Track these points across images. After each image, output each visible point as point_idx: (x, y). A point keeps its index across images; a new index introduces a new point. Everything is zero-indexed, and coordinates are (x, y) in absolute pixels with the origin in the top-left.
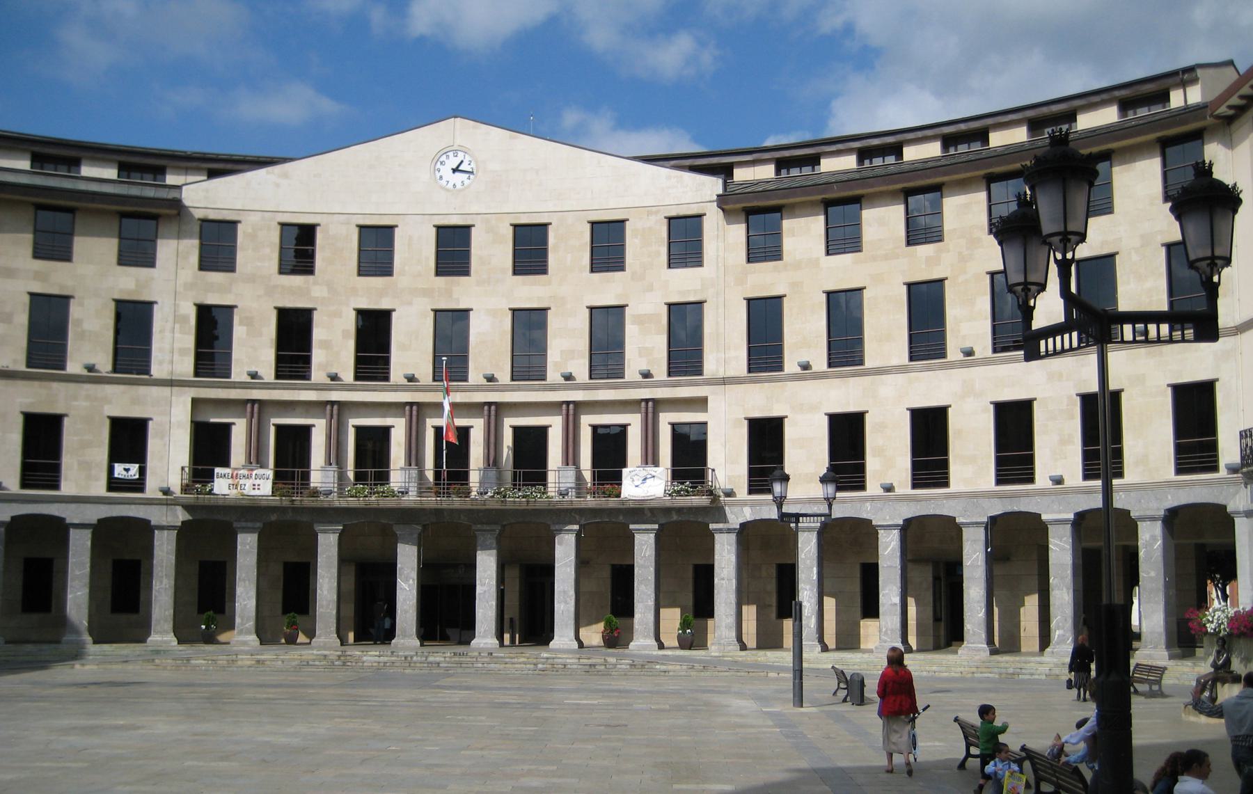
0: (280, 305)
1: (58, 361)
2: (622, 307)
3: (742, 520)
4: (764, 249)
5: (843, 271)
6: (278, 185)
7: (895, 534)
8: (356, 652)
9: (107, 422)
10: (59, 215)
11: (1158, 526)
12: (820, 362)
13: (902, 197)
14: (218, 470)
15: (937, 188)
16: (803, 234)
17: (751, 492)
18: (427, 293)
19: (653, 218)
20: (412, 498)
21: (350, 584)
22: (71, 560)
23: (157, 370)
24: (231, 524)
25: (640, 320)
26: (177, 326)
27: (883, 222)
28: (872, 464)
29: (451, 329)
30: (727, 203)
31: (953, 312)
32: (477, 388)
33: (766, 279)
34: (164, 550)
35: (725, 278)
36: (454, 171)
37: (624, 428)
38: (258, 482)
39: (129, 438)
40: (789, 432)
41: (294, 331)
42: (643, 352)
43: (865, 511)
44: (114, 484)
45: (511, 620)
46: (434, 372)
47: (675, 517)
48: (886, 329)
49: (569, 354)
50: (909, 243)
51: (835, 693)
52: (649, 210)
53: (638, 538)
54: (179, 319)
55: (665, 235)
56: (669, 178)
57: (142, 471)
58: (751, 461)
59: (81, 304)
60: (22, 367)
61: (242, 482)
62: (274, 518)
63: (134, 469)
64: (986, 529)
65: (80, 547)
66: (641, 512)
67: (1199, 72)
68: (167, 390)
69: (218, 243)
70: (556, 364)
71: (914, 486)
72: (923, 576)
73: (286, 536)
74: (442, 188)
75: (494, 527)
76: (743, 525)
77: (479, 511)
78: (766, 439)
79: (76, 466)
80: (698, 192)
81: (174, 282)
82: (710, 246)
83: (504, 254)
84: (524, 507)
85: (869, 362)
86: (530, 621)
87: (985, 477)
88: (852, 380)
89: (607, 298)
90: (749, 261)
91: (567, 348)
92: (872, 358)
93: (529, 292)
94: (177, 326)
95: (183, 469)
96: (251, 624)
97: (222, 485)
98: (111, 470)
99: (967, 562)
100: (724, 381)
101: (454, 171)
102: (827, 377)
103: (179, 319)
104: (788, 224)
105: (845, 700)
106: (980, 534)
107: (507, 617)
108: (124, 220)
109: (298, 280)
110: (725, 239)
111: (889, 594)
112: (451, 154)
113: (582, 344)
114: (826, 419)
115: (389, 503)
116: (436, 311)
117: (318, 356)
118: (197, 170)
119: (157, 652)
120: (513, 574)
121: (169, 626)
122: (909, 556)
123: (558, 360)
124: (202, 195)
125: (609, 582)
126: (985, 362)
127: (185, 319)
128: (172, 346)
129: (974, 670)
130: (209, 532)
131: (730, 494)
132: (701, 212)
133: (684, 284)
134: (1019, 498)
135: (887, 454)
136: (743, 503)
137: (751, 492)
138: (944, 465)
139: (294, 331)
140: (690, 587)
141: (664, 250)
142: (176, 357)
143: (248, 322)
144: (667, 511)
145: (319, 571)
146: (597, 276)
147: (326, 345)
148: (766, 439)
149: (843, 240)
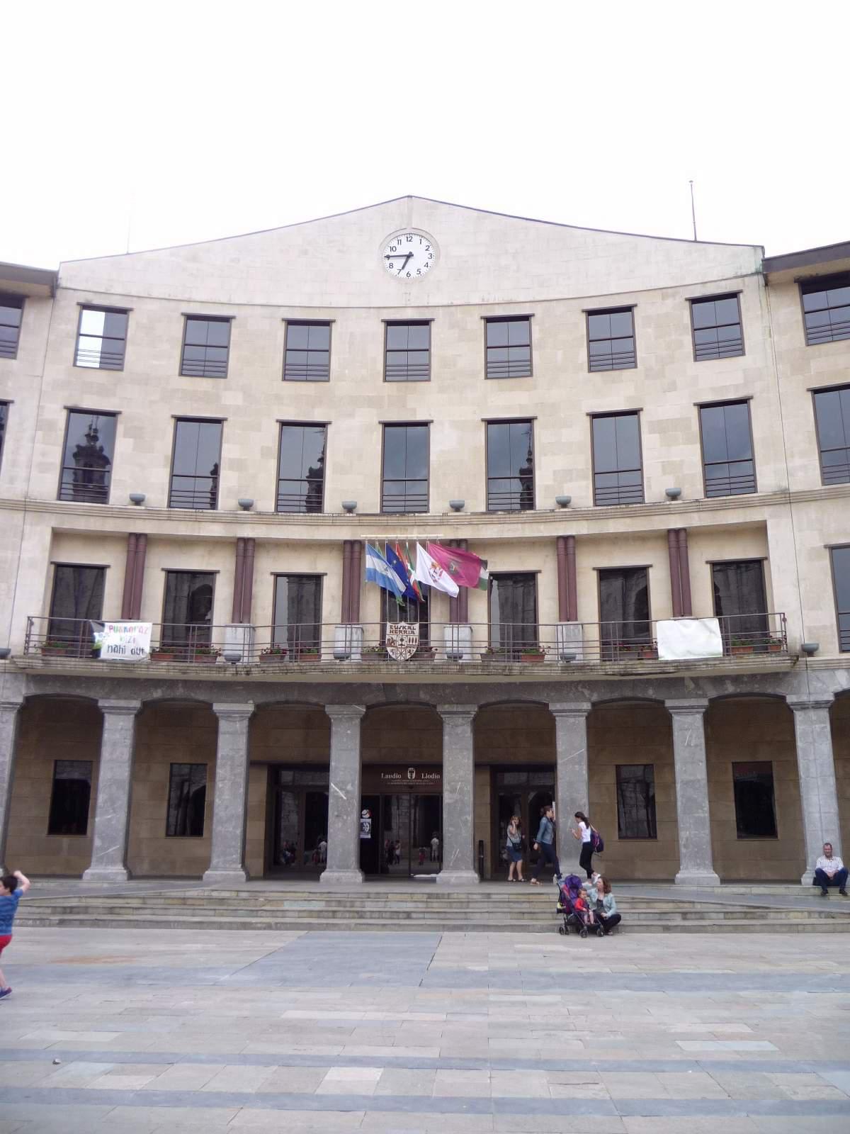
18: (372, 402)
19: (669, 302)
25: (661, 427)
36: (409, 256)
47: (730, 689)
53: (678, 721)
54: (42, 425)
62: (157, 694)
66: (681, 678)
75: (468, 708)
83: (473, 355)
96: (116, 848)
100: (786, 498)
101: (409, 256)
103: (42, 425)
112: (403, 239)
115: (314, 677)
127: (51, 425)
131: (809, 651)
136: (831, 667)
142: (34, 473)
143: (136, 433)
144: (718, 680)
146: (597, 376)
147: (239, 465)
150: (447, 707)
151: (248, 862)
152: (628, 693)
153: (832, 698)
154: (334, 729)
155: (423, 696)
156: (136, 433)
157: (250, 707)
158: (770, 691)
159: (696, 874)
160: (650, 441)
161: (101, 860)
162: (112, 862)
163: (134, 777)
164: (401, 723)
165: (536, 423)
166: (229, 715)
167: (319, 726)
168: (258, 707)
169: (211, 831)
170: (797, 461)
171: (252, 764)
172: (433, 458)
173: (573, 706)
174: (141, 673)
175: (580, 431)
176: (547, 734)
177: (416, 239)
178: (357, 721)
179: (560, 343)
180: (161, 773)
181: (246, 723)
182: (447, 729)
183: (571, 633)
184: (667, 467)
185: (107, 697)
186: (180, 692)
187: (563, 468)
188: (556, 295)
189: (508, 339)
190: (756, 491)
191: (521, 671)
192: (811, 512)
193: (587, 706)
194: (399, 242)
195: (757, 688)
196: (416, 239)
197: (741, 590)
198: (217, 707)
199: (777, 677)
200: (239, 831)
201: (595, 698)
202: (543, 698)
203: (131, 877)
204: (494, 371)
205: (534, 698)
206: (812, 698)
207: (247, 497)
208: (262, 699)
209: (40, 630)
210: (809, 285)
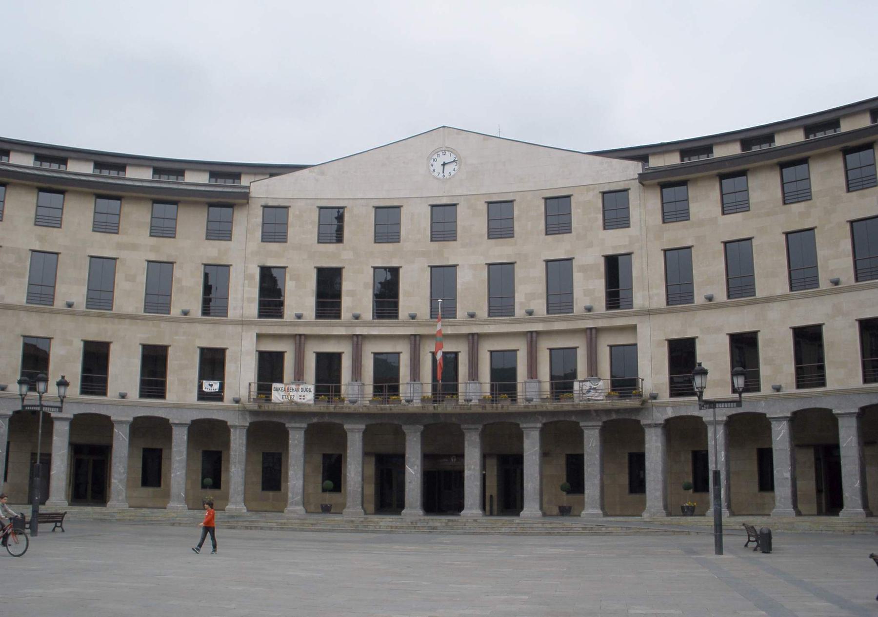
0: (319, 265)
1: (166, 308)
2: (571, 259)
3: (666, 417)
4: (675, 213)
5: (736, 226)
8: (376, 518)
9: (198, 351)
10: (168, 206)
12: (720, 294)
13: (778, 168)
14: (275, 385)
15: (804, 161)
16: (704, 201)
20: (417, 405)
21: (371, 470)
22: (174, 449)
23: (232, 314)
25: (584, 269)
26: (246, 282)
27: (764, 188)
29: (443, 279)
30: (646, 180)
32: (463, 324)
33: (678, 235)
34: (238, 443)
35: (645, 237)
38: (303, 394)
39: (213, 363)
41: (329, 286)
43: (761, 408)
44: (203, 396)
45: (491, 496)
46: (431, 312)
47: (614, 416)
48: (770, 270)
50: (785, 203)
51: (746, 545)
52: (588, 187)
53: (587, 433)
55: (601, 205)
57: (222, 387)
60: (142, 313)
61: (292, 394)
62: (315, 420)
63: (216, 386)
64: (857, 417)
65: (180, 438)
67: (717, 405)
68: (239, 328)
69: (275, 223)
70: (521, 303)
71: (798, 387)
72: (808, 457)
73: (326, 435)
74: (435, 178)
75: (477, 426)
76: (668, 421)
77: (466, 414)
81: (244, 255)
82: (635, 214)
83: (480, 225)
85: (759, 294)
86: (507, 499)
88: (746, 307)
89: (560, 254)
90: (664, 222)
91: (529, 292)
92: (762, 289)
93: (501, 251)
95: (250, 384)
96: (299, 498)
97: (278, 395)
98: (200, 386)
99: (843, 444)
102: (728, 306)
103: (248, 277)
104: (693, 192)
105: (755, 550)
106: (853, 422)
107: (488, 494)
108: (211, 209)
109: (332, 247)
110: (645, 208)
111: (782, 471)
112: (441, 153)
113: (541, 288)
116: (432, 267)
117: (346, 302)
118: (263, 174)
119: (233, 517)
120: (492, 464)
121: (240, 498)
122: (798, 442)
123: (523, 300)
124: (262, 190)
125: (564, 467)
126: (850, 289)
127: (251, 277)
128: (244, 296)
129: (854, 528)
131: (654, 397)
132: (626, 187)
133: (615, 241)
135: (777, 363)
136: (664, 406)
137: (672, 395)
139: (329, 286)
140: (627, 470)
141: (600, 216)
142: (245, 304)
144: (608, 412)
145: (348, 460)
146: (550, 238)
147: (352, 293)
150: (466, 426)
151: (365, 505)
154: (407, 438)
155: (454, 420)
157: (363, 427)
158: (634, 418)
159: (295, 509)
160: (577, 276)
161: (292, 504)
162: (297, 504)
163: (305, 462)
164: (443, 438)
165: (516, 265)
166: (352, 430)
167: (400, 435)
168: (367, 426)
169: (345, 490)
171: (366, 454)
172: (459, 286)
175: (540, 271)
176: (519, 437)
177: (448, 153)
178: (419, 434)
179: (530, 219)
180: (318, 459)
181: (361, 434)
182: (467, 438)
184: (587, 293)
185: (289, 423)
186: (326, 420)
187: (529, 292)
188: (527, 185)
189: (500, 219)
190: (632, 308)
191: (505, 406)
192: (657, 320)
193: (539, 425)
194: (439, 155)
195: (627, 416)
196: (448, 153)
198: (346, 427)
199: (637, 410)
200: (360, 490)
201: (544, 421)
202: (518, 421)
203: (307, 512)
204: (493, 234)
205: (513, 421)
206: (654, 422)
207: (357, 312)
208: (369, 422)
209: (254, 388)
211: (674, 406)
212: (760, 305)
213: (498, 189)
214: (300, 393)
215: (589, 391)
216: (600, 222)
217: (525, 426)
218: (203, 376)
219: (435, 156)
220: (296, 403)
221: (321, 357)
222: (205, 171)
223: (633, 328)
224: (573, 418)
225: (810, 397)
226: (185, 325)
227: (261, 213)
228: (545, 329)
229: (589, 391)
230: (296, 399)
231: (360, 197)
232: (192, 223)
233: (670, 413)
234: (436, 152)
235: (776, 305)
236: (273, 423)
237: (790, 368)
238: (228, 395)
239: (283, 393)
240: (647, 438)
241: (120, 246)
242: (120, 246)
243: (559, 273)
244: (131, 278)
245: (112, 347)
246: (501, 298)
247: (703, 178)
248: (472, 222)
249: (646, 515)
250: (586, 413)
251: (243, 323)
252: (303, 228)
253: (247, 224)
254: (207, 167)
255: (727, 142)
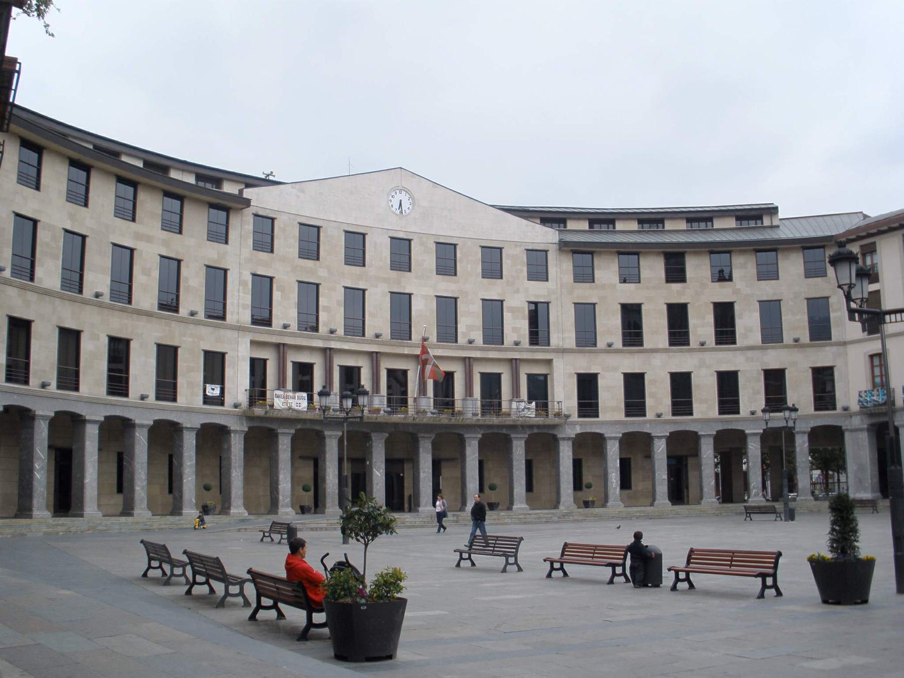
4: (584, 275)
6: (298, 197)
7: (664, 441)
9: (202, 354)
10: (817, 250)
11: (806, 438)
12: (618, 343)
16: (607, 271)
17: (580, 416)
18: (385, 280)
19: (518, 249)
24: (321, 432)
25: (513, 310)
28: (649, 401)
31: (692, 321)
35: (560, 289)
37: (483, 375)
38: (299, 401)
39: (215, 366)
40: (601, 382)
42: (515, 330)
43: (646, 429)
44: (207, 400)
47: (536, 431)
49: (471, 328)
52: (516, 244)
56: (527, 226)
58: (579, 399)
59: (188, 267)
61: (290, 401)
70: (463, 333)
73: (308, 437)
74: (394, 213)
78: (587, 386)
79: (185, 386)
80: (545, 236)
81: (239, 257)
84: (402, 421)
87: (713, 411)
91: (470, 324)
94: (241, 288)
96: (288, 500)
100: (564, 351)
103: (242, 283)
110: (561, 269)
114: (622, 376)
121: (240, 502)
126: (712, 350)
127: (245, 283)
130: (636, 445)
131: (567, 416)
133: (538, 291)
134: (731, 422)
135: (658, 397)
136: (574, 424)
137: (580, 416)
138: (690, 404)
143: (282, 289)
147: (328, 309)
148: (587, 386)
149: (629, 277)
152: (496, 431)
153: (103, 419)
156: (282, 289)
159: (520, 504)
160: (507, 315)
161: (283, 506)
162: (287, 506)
166: (330, 437)
170: (566, 335)
173: (474, 436)
174: (303, 417)
175: (477, 308)
177: (403, 193)
183: (468, 403)
187: (470, 324)
196: (403, 193)
197: (539, 389)
207: (333, 327)
210: (574, 252)
211: (581, 424)
212: (647, 355)
213: (448, 233)
214: (296, 401)
215: (523, 410)
216: (525, 273)
217: (468, 436)
218: (208, 380)
219: (393, 194)
220: (294, 410)
221: (531, 378)
222: (634, 219)
223: (549, 362)
224: (504, 431)
225: (681, 422)
226: (191, 326)
227: (252, 221)
228: (478, 356)
229: (523, 410)
230: (294, 406)
231: (336, 219)
232: (197, 220)
233: (578, 430)
234: (394, 189)
235: (658, 356)
236: (267, 428)
237: (667, 401)
238: (229, 400)
239: (282, 400)
240: (561, 448)
241: (138, 237)
242: (138, 237)
243: (493, 311)
244: (147, 272)
245: (133, 345)
246: (448, 328)
247: (605, 252)
248: (424, 257)
249: (561, 507)
250: (514, 427)
251: (239, 328)
252: (287, 242)
253: (242, 228)
254: (635, 216)
255: (579, 219)
